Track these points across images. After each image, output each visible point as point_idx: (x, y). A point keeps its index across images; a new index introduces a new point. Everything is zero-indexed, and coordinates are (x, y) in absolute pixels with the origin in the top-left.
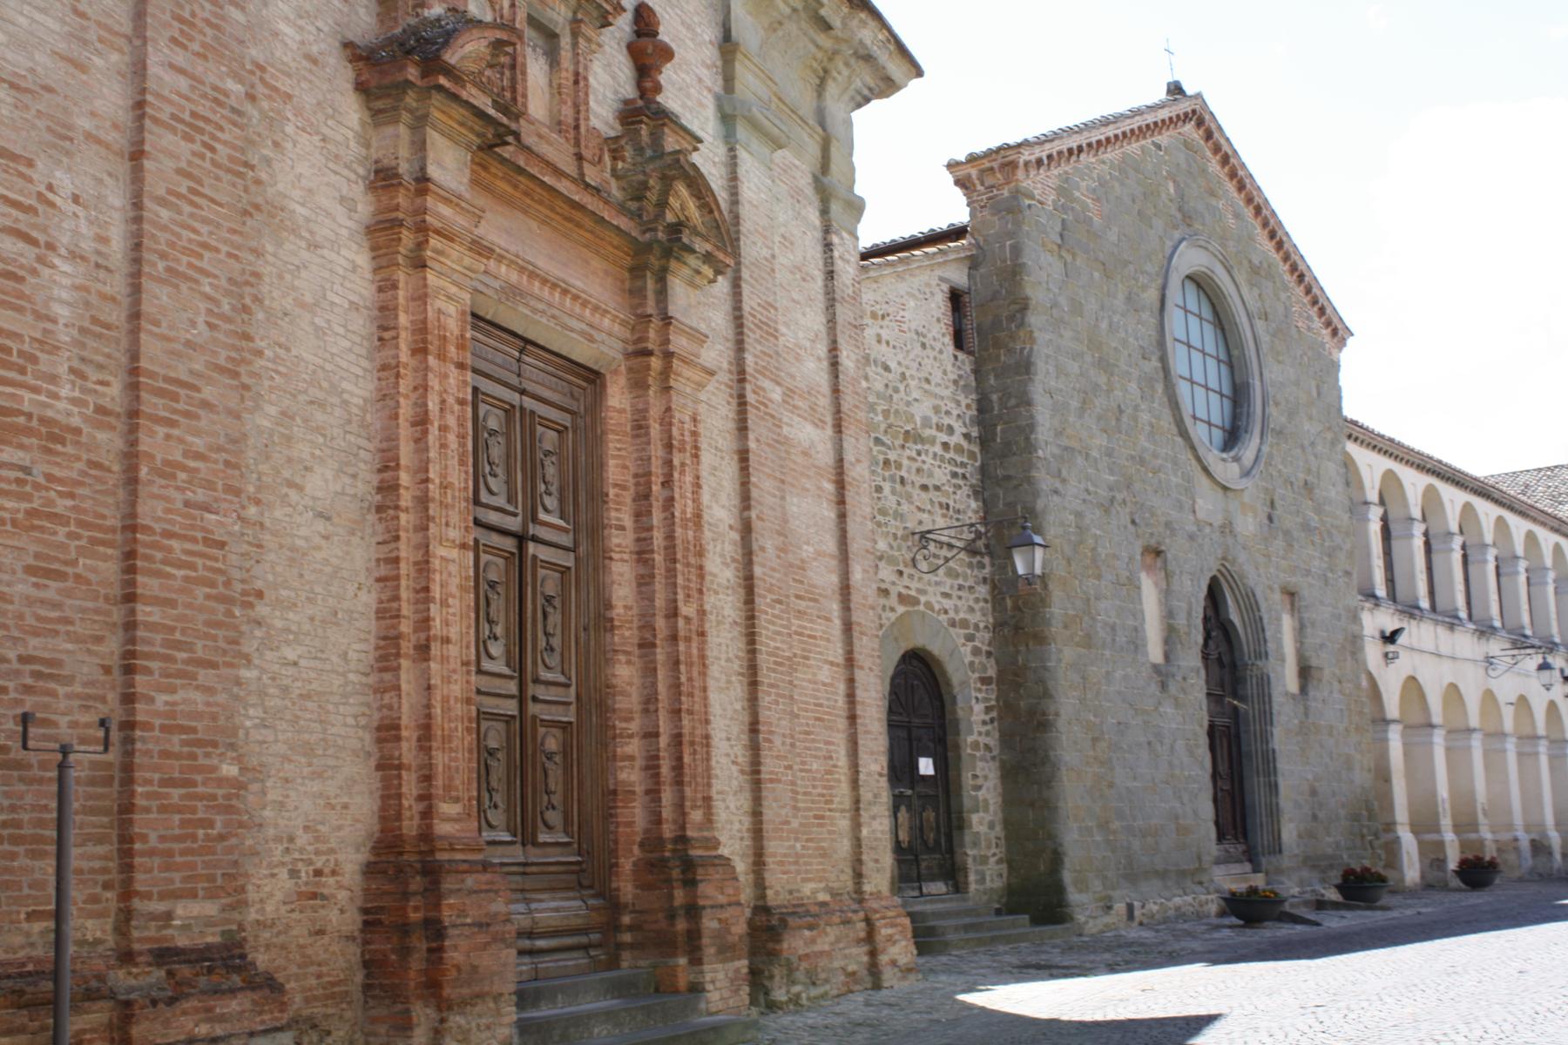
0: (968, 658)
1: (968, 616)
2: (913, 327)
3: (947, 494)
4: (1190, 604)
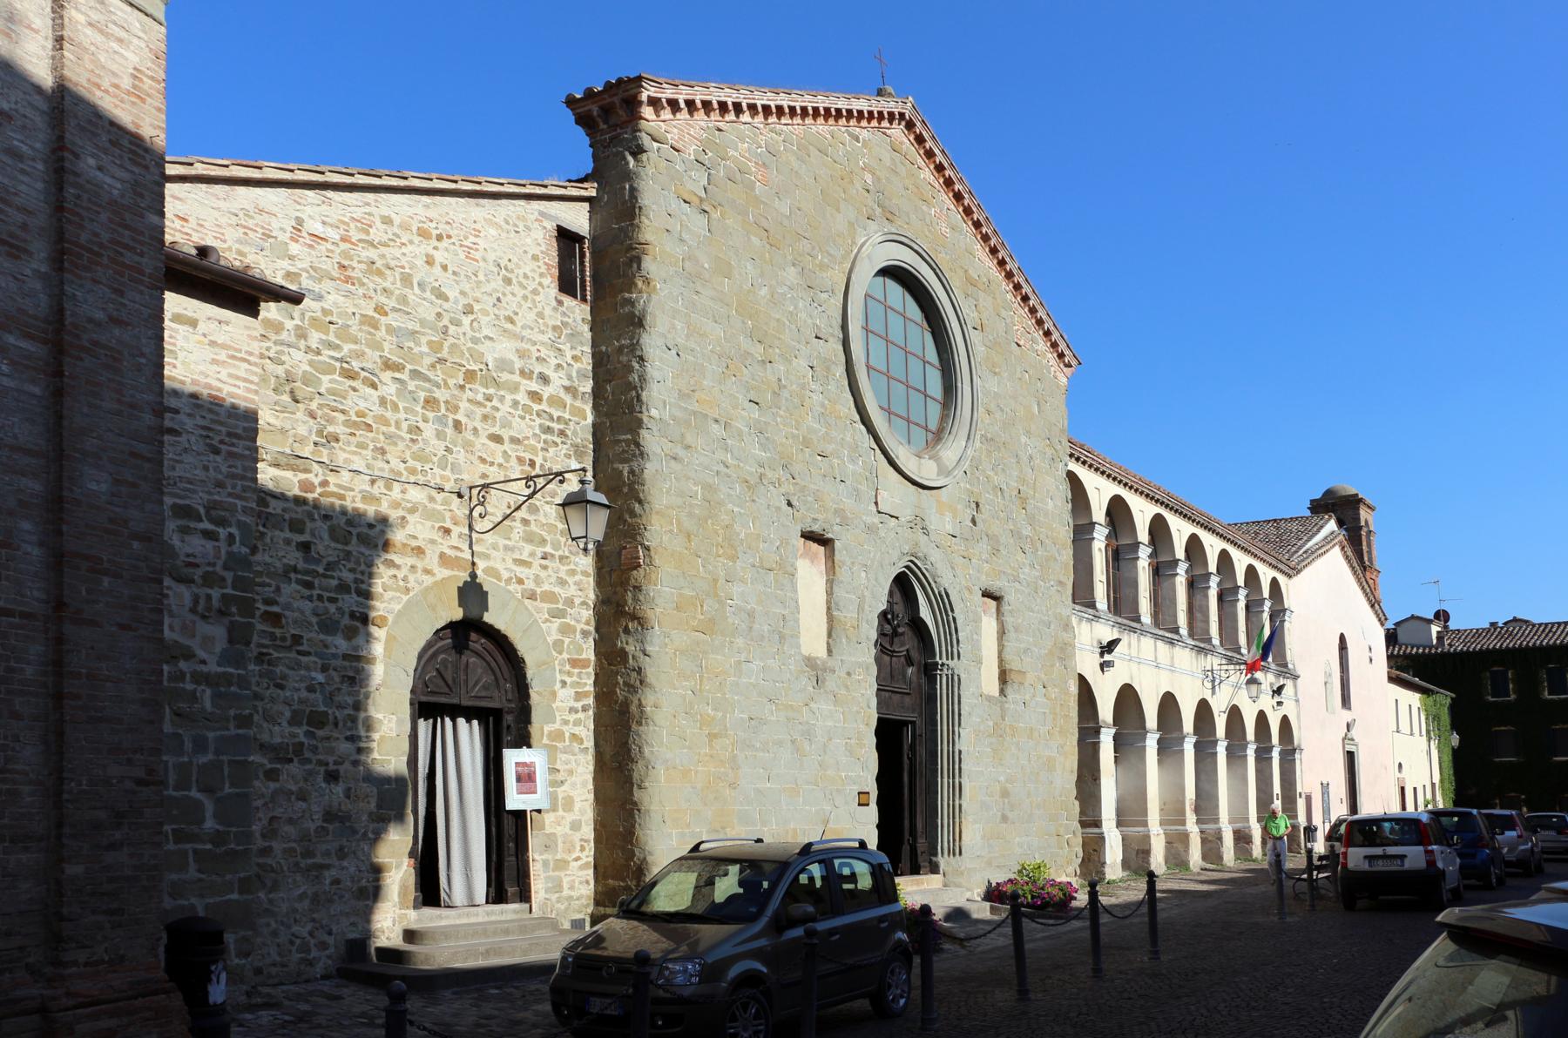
0: (554, 636)
1: (557, 590)
2: (491, 256)
3: (534, 450)
4: (862, 598)
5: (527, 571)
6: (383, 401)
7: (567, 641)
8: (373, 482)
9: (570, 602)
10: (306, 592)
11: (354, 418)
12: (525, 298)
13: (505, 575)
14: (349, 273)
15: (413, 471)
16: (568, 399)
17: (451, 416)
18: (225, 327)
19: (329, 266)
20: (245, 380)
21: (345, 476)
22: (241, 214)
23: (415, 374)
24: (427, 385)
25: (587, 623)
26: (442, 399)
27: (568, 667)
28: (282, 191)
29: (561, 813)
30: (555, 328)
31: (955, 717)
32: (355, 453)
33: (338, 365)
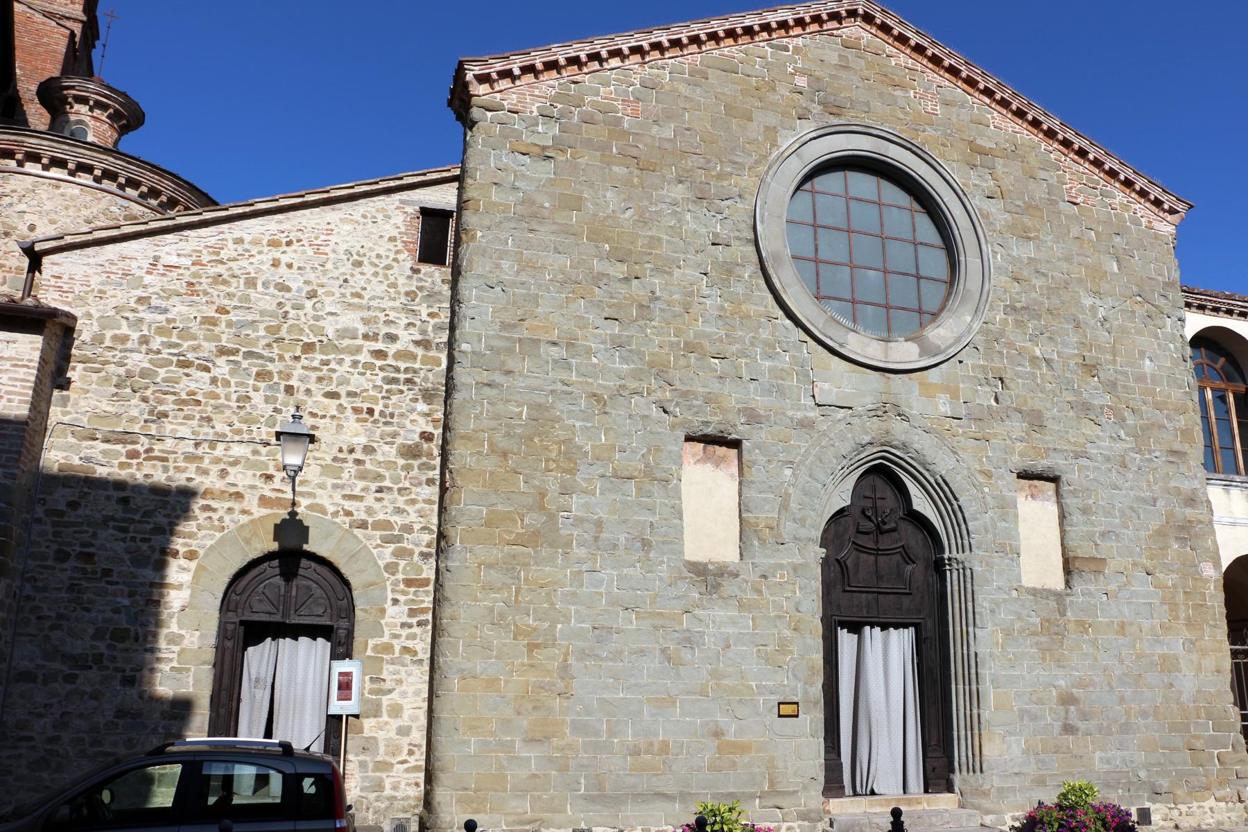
2: (343, 247)
5: (358, 504)
6: (214, 381)
7: (402, 563)
8: (197, 445)
9: (408, 529)
10: (122, 535)
11: (184, 396)
12: (376, 274)
13: (331, 509)
14: (197, 287)
15: (239, 432)
16: (420, 352)
17: (283, 383)
18: (11, 345)
19: (180, 287)
20: (23, 380)
21: (169, 444)
22: (107, 264)
23: (249, 355)
24: (260, 361)
25: (428, 546)
26: (275, 371)
27: (402, 586)
28: (144, 241)
29: (385, 718)
30: (407, 294)
31: (970, 617)
32: (181, 424)
33: (175, 359)
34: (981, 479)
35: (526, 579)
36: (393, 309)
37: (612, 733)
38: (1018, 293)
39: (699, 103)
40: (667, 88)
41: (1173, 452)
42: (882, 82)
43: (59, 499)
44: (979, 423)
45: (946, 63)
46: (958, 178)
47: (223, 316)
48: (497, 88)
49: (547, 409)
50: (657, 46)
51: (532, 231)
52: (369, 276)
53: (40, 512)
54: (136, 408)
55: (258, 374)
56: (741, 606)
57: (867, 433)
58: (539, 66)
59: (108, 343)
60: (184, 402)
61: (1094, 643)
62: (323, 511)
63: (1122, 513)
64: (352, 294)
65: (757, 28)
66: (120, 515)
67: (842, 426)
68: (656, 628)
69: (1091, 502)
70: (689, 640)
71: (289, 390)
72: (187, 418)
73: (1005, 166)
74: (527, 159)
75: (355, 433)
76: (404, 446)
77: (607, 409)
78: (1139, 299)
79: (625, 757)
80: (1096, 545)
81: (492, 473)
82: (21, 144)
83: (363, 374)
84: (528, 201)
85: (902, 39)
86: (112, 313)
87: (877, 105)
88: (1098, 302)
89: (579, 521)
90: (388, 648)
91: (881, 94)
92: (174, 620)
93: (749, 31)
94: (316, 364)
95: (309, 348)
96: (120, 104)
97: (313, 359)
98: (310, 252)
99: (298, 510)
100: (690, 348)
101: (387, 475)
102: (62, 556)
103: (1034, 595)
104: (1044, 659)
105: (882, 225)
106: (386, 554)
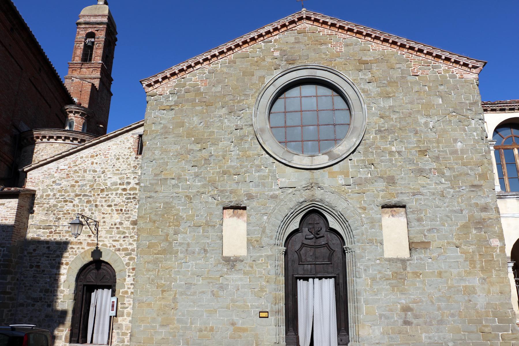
7: (131, 262)
11: (65, 212)
12: (124, 162)
13: (109, 245)
14: (70, 175)
19: (65, 176)
21: (61, 227)
23: (84, 195)
27: (131, 271)
29: (125, 317)
30: (134, 167)
34: (360, 211)
35: (161, 267)
36: (129, 173)
37: (192, 323)
38: (383, 124)
39: (231, 74)
40: (219, 71)
41: (473, 186)
42: (315, 44)
43: (31, 247)
44: (360, 186)
45: (346, 28)
46: (350, 79)
47: (77, 184)
48: (155, 88)
49: (170, 204)
50: (214, 56)
51: (165, 138)
52: (121, 163)
53: (26, 253)
54: (52, 217)
55: (87, 202)
56: (245, 273)
57: (302, 197)
58: (169, 76)
59: (44, 197)
60: (65, 214)
61: (423, 282)
62: (106, 246)
63: (441, 219)
64: (116, 170)
65: (256, 37)
66: (47, 252)
67: (291, 196)
68: (209, 283)
69: (422, 215)
70: (221, 287)
71: (96, 206)
72: (66, 219)
73: (377, 66)
74: (165, 111)
75: (116, 218)
76: (132, 221)
77: (192, 201)
78: (454, 114)
79: (196, 332)
80: (425, 235)
81: (150, 229)
82: (40, 134)
83: (119, 197)
84: (165, 127)
85: (325, 23)
86: (46, 187)
87: (312, 55)
88: (429, 120)
89: (181, 244)
90: (126, 292)
91: (314, 50)
92: (62, 285)
93: (253, 39)
94: (104, 196)
95: (102, 190)
96: (83, 110)
97: (103, 195)
98: (103, 157)
99: (99, 246)
100: (224, 173)
101: (127, 232)
102: (31, 267)
103: (389, 261)
104: (393, 290)
105: (317, 105)
106: (126, 260)
